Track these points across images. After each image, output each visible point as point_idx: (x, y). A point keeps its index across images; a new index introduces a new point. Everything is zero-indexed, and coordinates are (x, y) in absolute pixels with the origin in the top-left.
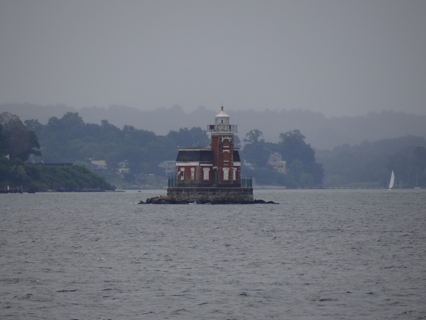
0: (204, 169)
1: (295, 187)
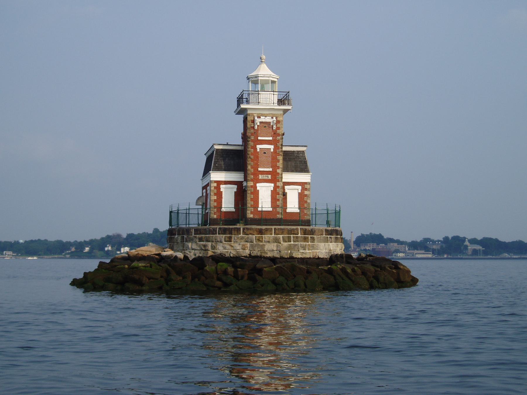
0: (223, 187)
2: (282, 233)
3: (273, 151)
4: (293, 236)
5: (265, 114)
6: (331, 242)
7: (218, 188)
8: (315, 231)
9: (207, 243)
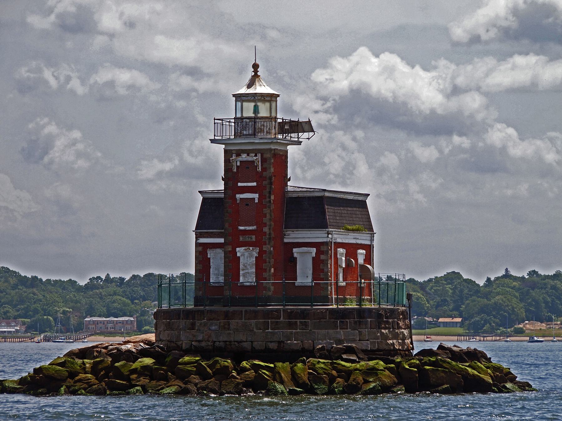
0: (210, 254)
1: (15, 272)
2: (255, 318)
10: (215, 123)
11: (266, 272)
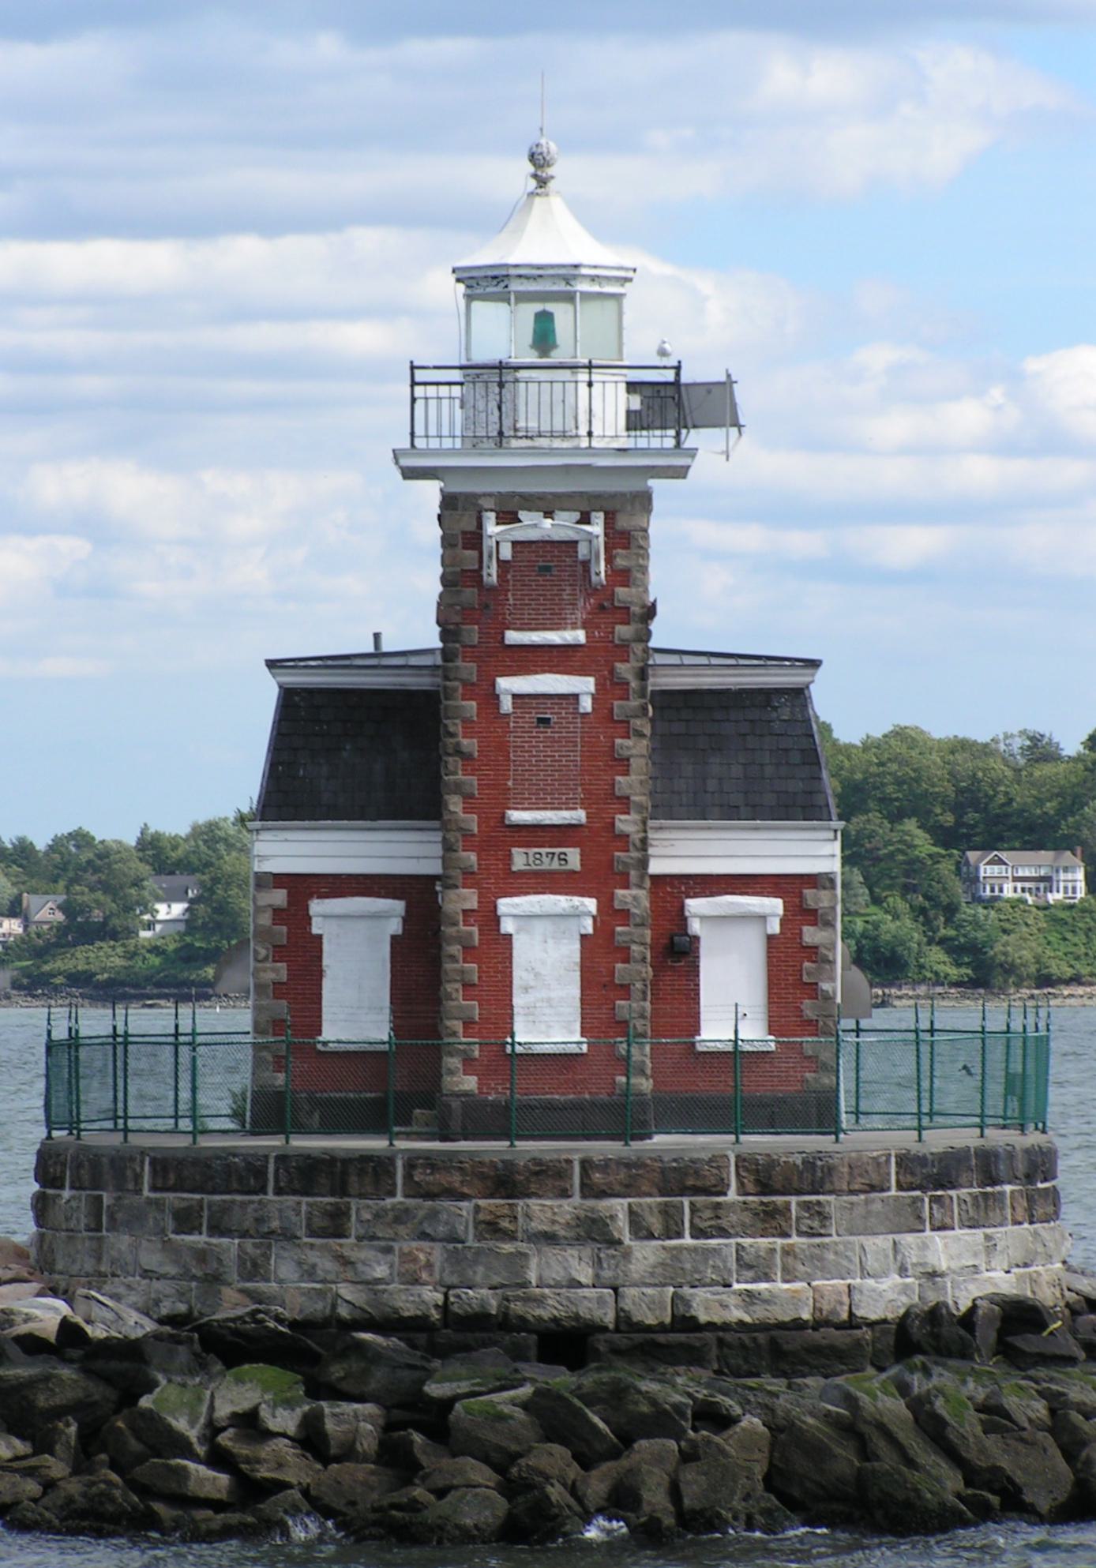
3: (589, 709)
4: (692, 1204)
5: (541, 497)
6: (943, 1227)
7: (295, 916)
8: (830, 1170)
9: (214, 1241)
10: (413, 400)
11: (627, 997)
